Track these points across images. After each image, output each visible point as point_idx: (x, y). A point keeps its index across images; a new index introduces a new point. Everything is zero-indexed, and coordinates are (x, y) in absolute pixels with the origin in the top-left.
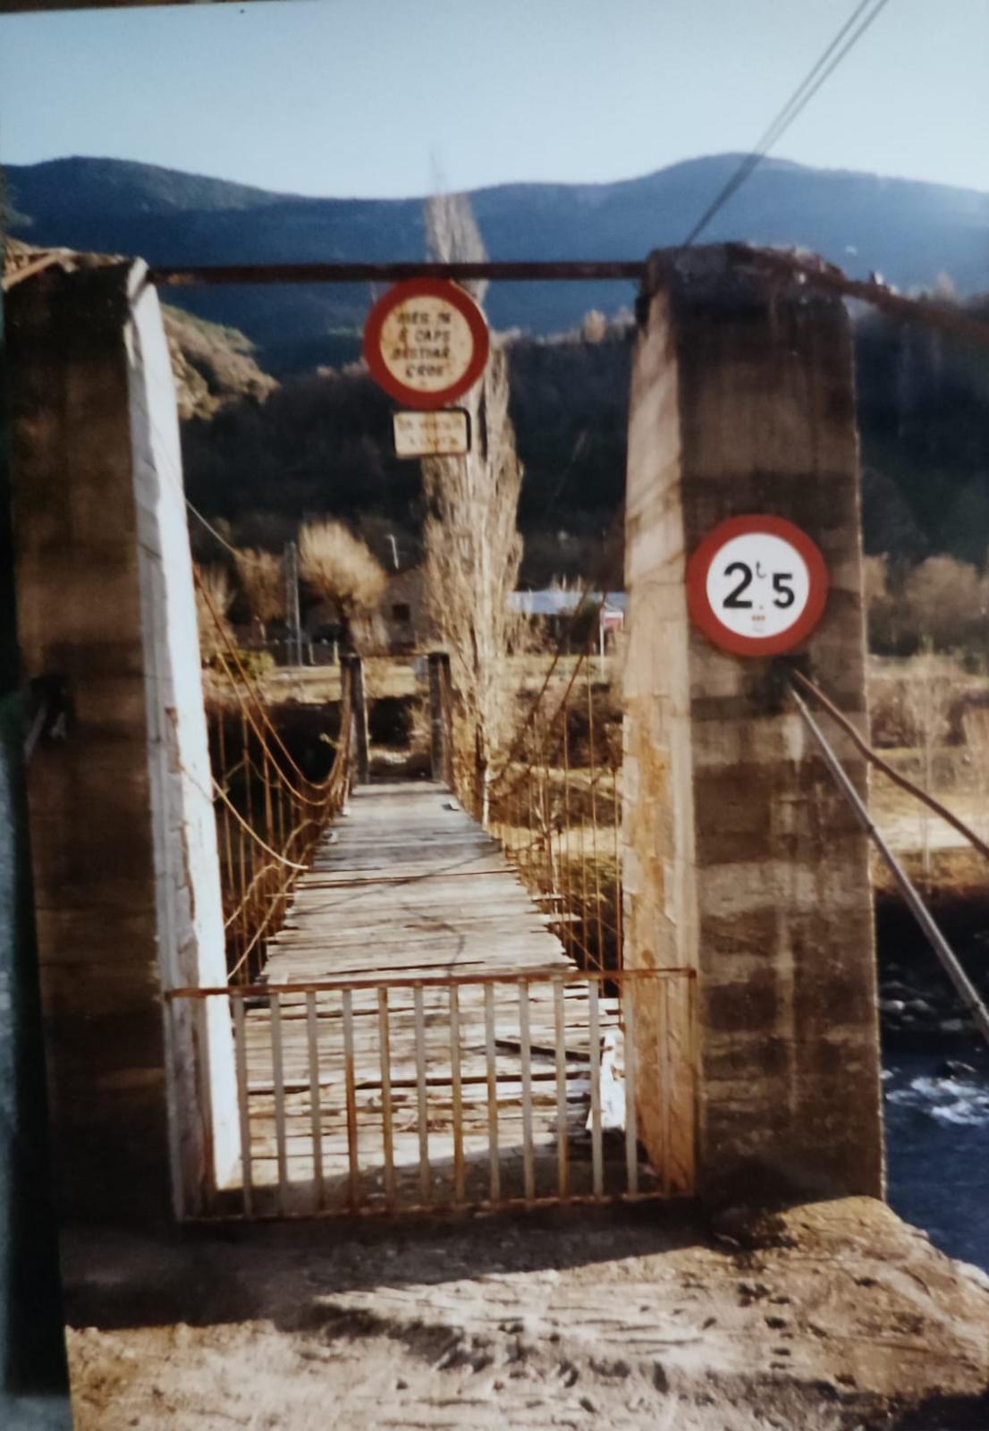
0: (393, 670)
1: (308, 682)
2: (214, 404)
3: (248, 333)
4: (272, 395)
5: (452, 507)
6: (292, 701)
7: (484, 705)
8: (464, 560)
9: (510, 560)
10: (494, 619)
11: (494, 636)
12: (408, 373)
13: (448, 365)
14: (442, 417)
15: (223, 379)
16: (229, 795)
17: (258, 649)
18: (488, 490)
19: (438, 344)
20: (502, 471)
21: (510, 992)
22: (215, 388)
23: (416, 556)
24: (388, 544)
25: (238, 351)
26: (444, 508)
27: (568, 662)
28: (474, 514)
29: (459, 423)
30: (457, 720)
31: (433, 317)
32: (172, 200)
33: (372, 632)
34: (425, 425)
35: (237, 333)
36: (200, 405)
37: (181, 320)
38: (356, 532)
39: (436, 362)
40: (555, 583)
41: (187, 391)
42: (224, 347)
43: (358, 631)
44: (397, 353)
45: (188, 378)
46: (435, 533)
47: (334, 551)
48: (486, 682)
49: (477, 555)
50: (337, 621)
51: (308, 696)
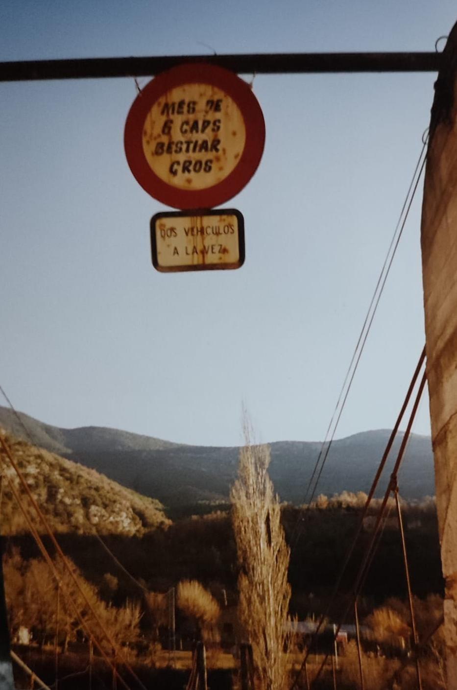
0: (222, 656)
1: (179, 659)
2: (144, 531)
3: (161, 501)
4: (170, 527)
5: (253, 569)
6: (169, 668)
7: (271, 674)
8: (258, 595)
9: (284, 598)
10: (277, 628)
11: (277, 639)
12: (173, 172)
13: (218, 159)
14: (211, 222)
15: (150, 521)
16: (29, 676)
17: (154, 640)
18: (271, 560)
19: (207, 135)
20: (279, 551)
21: (211, 258)
22: (145, 524)
23: (234, 591)
24: (223, 595)
25: (157, 509)
26: (249, 569)
27: (319, 658)
28: (264, 572)
29: (230, 226)
30: (256, 682)
31: (202, 105)
32: (131, 445)
33: (213, 635)
34: (190, 232)
35: (157, 501)
36: (138, 531)
37: (132, 494)
38: (206, 586)
39: (203, 156)
40: (309, 619)
41: (132, 524)
42: (151, 507)
43: (206, 635)
44: (160, 150)
45: (133, 519)
46: (245, 582)
47: (195, 595)
48: (273, 661)
49: (267, 593)
50: (195, 630)
51: (178, 666)
